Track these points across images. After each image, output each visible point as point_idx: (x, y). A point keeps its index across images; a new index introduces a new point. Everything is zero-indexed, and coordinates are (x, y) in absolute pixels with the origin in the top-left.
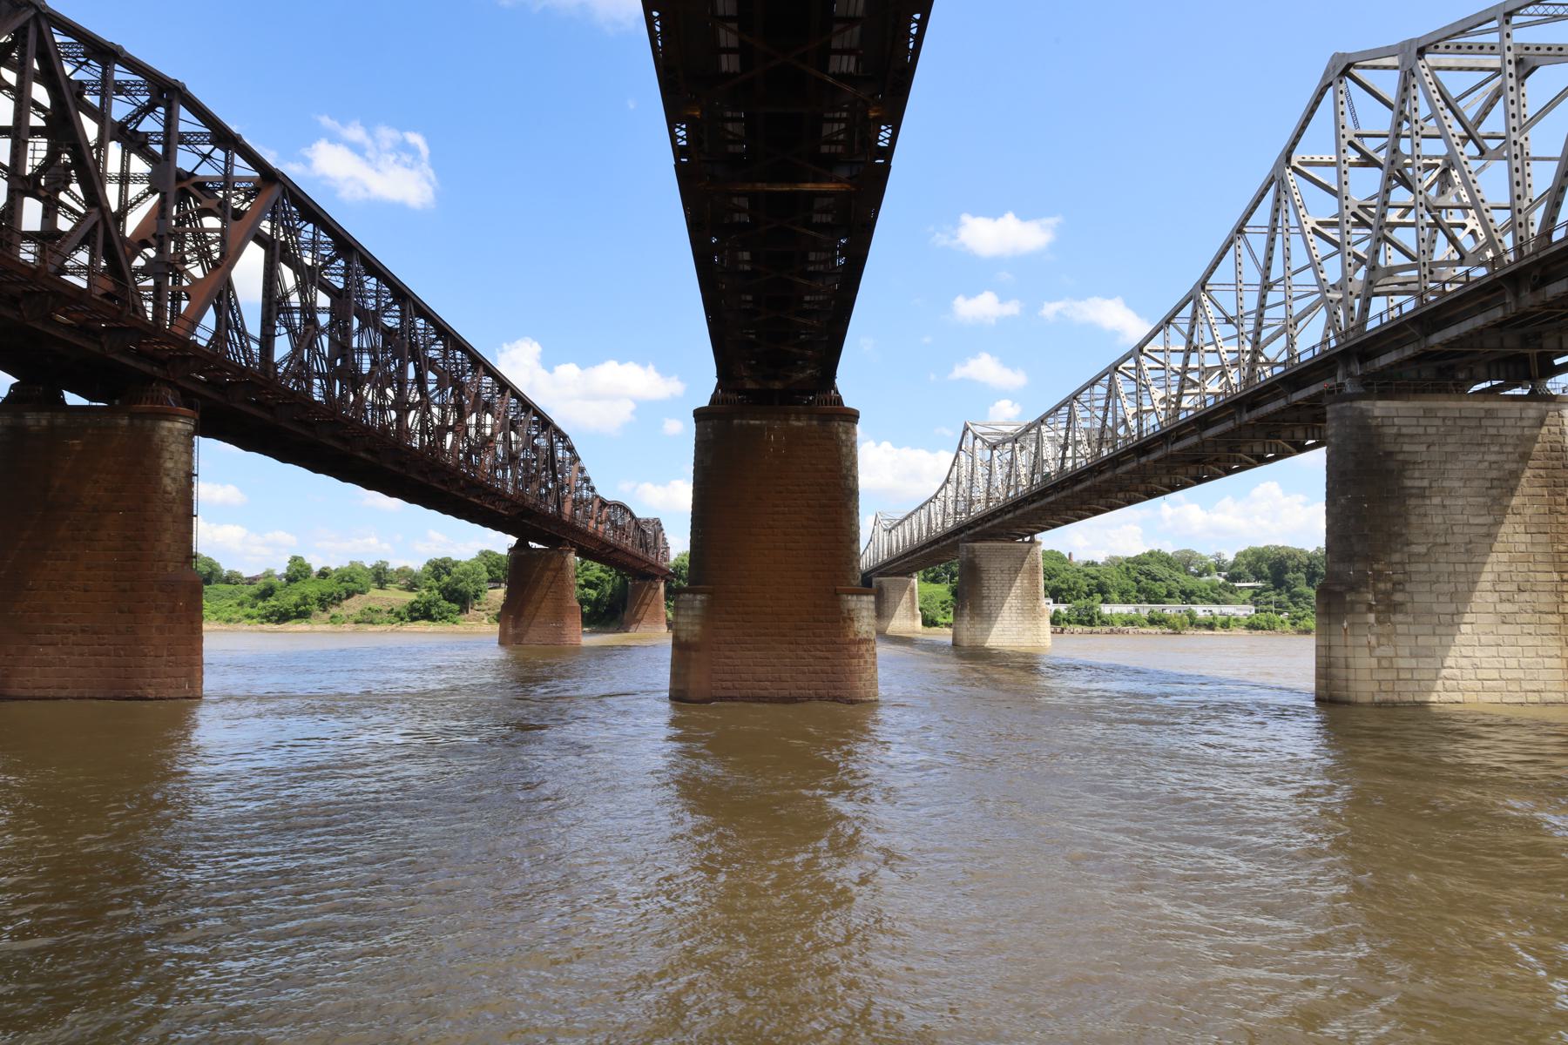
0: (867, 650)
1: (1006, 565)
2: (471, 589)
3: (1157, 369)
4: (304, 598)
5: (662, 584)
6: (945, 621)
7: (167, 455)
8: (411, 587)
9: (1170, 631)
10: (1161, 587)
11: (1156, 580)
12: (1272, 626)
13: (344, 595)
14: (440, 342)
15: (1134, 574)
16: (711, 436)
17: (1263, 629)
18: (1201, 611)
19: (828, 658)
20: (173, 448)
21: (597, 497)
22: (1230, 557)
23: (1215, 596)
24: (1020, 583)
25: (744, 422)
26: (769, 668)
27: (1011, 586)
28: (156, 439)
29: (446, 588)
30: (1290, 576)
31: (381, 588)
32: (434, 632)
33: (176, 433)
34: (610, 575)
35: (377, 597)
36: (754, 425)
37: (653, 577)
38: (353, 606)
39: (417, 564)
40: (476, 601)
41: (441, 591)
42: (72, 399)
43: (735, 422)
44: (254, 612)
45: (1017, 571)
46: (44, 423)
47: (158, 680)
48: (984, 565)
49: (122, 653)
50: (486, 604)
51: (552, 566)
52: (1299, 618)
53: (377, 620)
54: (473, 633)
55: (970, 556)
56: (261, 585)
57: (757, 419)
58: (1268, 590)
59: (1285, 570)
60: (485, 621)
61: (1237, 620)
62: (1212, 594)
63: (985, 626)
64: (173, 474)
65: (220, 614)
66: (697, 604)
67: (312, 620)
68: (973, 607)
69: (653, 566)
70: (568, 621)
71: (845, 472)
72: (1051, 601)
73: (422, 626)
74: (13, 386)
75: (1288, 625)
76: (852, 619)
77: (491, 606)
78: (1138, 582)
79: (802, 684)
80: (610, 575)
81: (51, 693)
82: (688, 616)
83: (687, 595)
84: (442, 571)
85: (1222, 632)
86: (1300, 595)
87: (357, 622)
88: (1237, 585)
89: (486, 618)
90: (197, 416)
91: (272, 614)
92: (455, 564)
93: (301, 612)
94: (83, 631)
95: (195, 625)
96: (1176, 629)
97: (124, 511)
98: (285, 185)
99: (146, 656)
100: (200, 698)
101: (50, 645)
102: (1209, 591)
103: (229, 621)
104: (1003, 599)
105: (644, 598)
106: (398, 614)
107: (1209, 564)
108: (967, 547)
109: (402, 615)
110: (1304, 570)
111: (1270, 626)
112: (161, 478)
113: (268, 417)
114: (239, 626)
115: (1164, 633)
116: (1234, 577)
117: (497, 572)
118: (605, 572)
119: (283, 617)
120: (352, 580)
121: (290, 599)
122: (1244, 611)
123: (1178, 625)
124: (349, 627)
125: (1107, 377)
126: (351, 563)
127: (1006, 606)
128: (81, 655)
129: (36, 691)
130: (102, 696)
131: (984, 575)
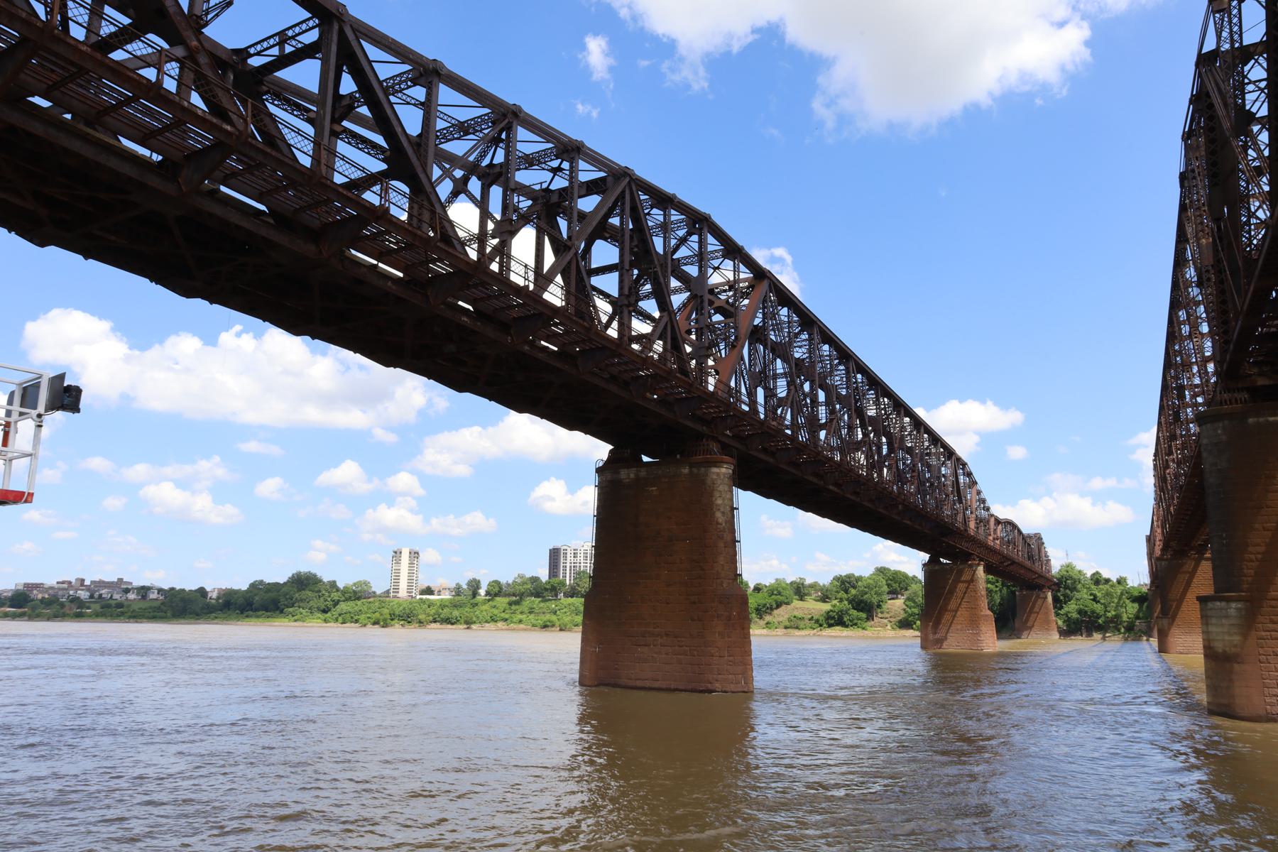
2: (875, 600)
5: (1050, 594)
7: (717, 494)
8: (824, 599)
13: (775, 606)
14: (873, 392)
16: (1224, 438)
20: (721, 488)
21: (992, 515)
25: (1261, 420)
28: (709, 482)
29: (853, 600)
31: (801, 600)
34: (997, 587)
35: (800, 607)
37: (1040, 588)
38: (782, 614)
39: (825, 580)
40: (879, 610)
41: (850, 602)
42: (645, 459)
43: (1251, 420)
46: (632, 476)
49: (695, 653)
50: (888, 613)
51: (963, 579)
53: (801, 626)
54: (881, 638)
60: (889, 627)
64: (722, 509)
66: (1232, 612)
69: (1042, 576)
70: (983, 628)
73: (837, 631)
74: (611, 451)
77: (892, 614)
80: (997, 587)
81: (648, 684)
82: (1222, 625)
83: (1218, 603)
84: (848, 585)
87: (786, 628)
89: (889, 625)
90: (735, 462)
92: (859, 579)
94: (667, 635)
98: (771, 280)
100: (752, 692)
101: (645, 645)
105: (1033, 607)
106: (817, 621)
109: (820, 622)
112: (714, 513)
113: (771, 460)
117: (894, 585)
118: (993, 583)
120: (779, 594)
124: (781, 631)
126: (777, 580)
128: (667, 654)
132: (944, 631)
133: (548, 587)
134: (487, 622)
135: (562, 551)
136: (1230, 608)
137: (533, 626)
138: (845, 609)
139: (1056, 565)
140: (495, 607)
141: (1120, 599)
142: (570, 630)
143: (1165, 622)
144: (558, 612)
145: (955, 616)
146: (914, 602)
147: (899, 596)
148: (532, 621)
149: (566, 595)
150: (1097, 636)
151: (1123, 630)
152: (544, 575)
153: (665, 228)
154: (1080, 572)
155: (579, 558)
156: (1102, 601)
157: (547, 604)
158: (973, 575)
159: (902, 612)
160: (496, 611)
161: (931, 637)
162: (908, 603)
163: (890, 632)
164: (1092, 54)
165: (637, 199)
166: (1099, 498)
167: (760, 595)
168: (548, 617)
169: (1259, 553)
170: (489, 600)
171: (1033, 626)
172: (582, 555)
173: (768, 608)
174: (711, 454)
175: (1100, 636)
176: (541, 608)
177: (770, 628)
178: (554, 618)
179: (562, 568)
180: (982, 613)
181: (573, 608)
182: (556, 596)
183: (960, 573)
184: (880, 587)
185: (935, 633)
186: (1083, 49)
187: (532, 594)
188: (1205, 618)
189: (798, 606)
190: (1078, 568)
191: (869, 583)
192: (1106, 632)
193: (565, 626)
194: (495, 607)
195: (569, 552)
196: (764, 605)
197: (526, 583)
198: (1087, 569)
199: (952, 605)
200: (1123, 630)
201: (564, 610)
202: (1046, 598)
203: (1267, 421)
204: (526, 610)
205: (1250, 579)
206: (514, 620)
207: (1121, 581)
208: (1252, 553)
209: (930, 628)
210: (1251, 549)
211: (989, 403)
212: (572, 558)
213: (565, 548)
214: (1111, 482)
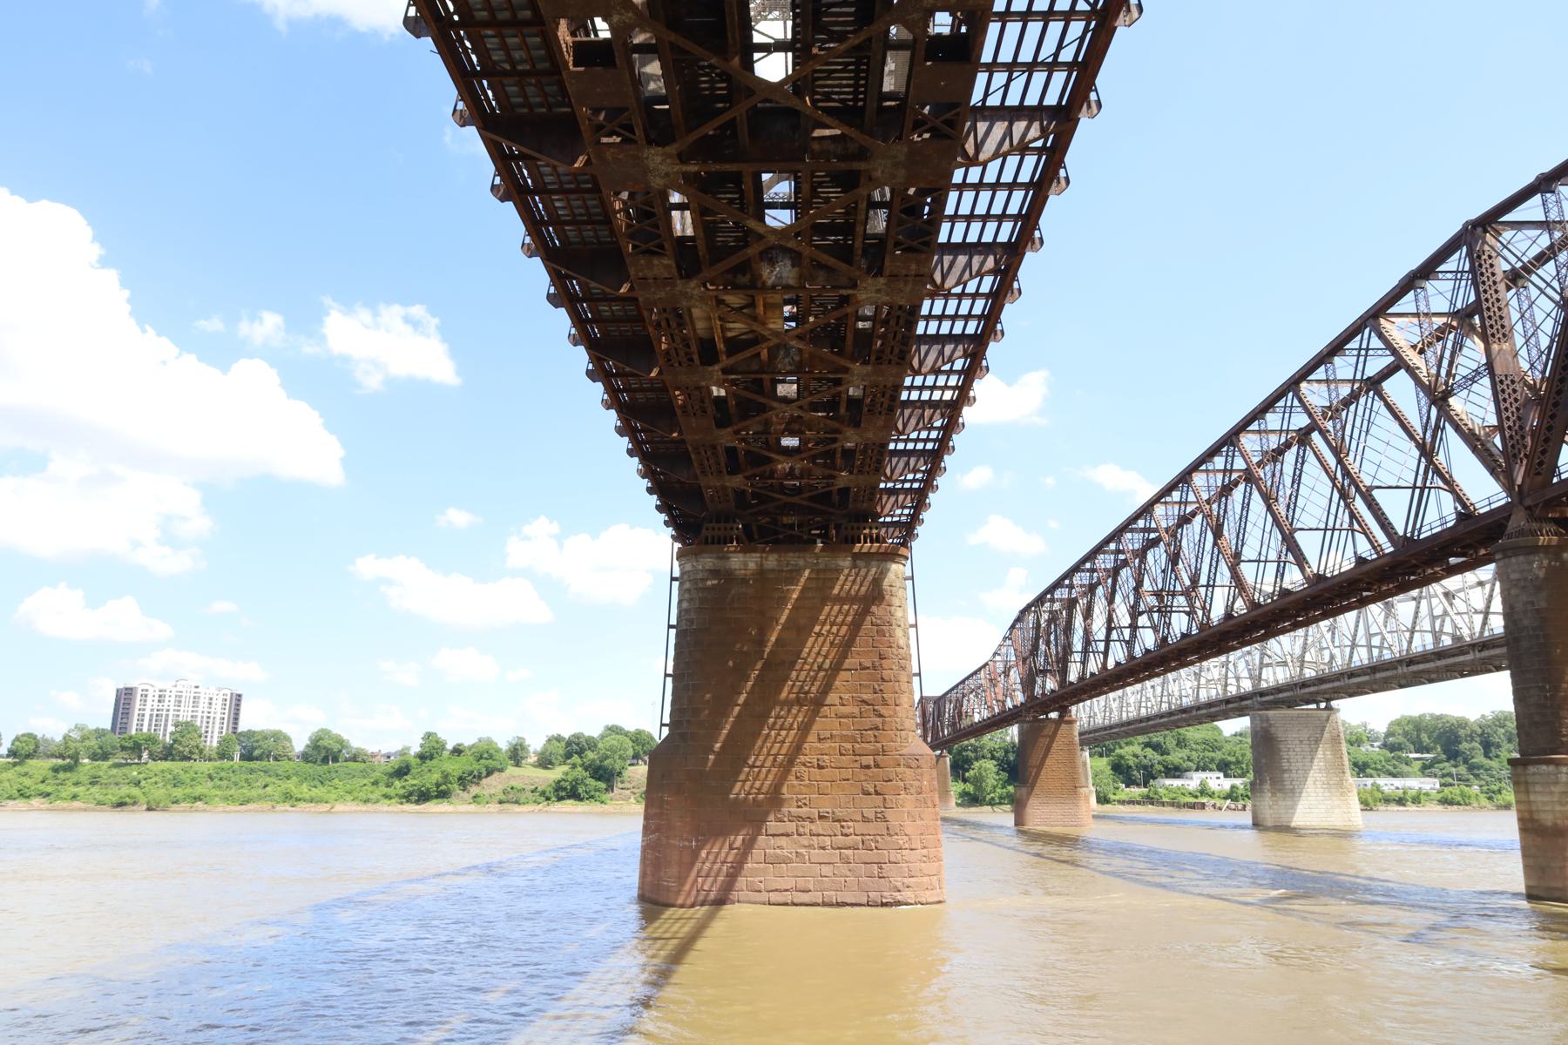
1: (1305, 734)
4: (446, 776)
6: (1117, 798)
12: (1467, 801)
13: (484, 773)
23: (1391, 768)
24: (1323, 754)
27: (1313, 759)
29: (590, 766)
30: (1464, 746)
38: (493, 785)
40: (619, 779)
44: (390, 791)
45: (1317, 742)
46: (752, 565)
48: (1280, 734)
49: (873, 845)
53: (522, 800)
55: (1265, 725)
56: (395, 762)
59: (1457, 740)
60: (632, 800)
61: (1427, 794)
63: (1289, 803)
65: (356, 794)
67: (453, 799)
68: (1274, 782)
72: (1221, 775)
73: (569, 805)
82: (1552, 793)
83: (1544, 767)
86: (1480, 767)
87: (501, 802)
91: (411, 794)
93: (442, 791)
101: (782, 835)
103: (367, 801)
104: (1306, 772)
106: (543, 793)
108: (1260, 715)
109: (547, 794)
110: (1478, 739)
114: (378, 807)
119: (423, 796)
121: (431, 779)
122: (1430, 784)
124: (494, 807)
127: (1310, 781)
131: (1281, 746)
133: (127, 744)
134: (10, 798)
135: (140, 692)
136: (1561, 773)
137: (99, 803)
140: (26, 774)
142: (165, 809)
144: (143, 783)
148: (97, 796)
149: (152, 757)
155: (166, 704)
157: (125, 770)
160: (27, 782)
167: (463, 759)
168: (125, 790)
170: (15, 765)
171: (775, 799)
172: (173, 699)
173: (474, 777)
177: (479, 803)
178: (135, 791)
179: (136, 717)
181: (170, 777)
182: (140, 757)
184: (626, 750)
188: (1520, 784)
189: (515, 774)
194: (26, 774)
195: (150, 694)
196: (471, 773)
201: (153, 780)
204: (85, 779)
206: (64, 795)
212: (156, 703)
213: (145, 687)
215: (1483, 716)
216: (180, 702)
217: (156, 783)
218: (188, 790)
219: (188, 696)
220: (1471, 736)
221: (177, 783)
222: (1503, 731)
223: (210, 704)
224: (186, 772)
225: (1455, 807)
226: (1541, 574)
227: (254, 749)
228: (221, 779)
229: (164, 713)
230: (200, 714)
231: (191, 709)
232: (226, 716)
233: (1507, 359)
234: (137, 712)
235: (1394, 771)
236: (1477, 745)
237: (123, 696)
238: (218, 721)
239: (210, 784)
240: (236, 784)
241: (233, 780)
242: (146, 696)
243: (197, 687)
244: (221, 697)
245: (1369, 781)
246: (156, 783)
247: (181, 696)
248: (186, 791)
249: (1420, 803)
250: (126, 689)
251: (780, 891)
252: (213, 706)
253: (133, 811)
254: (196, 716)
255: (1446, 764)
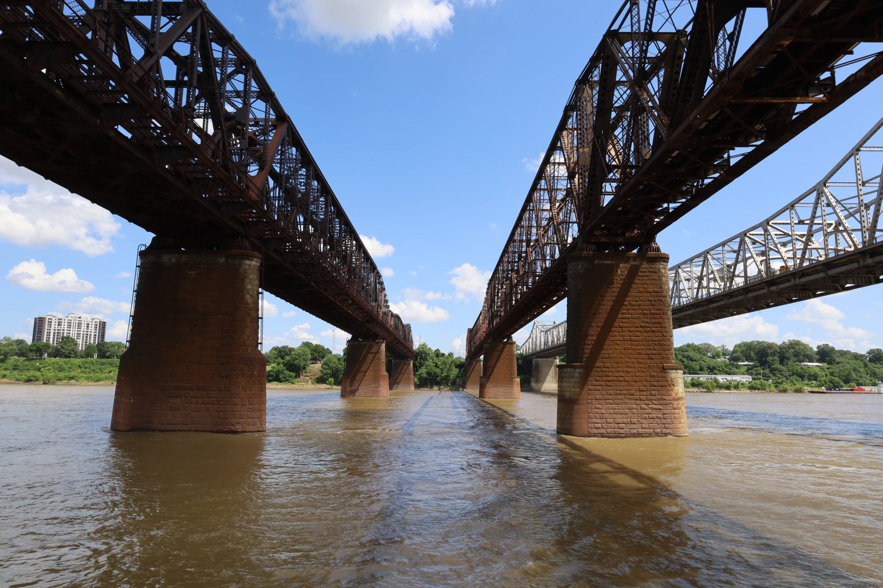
0: (682, 404)
2: (302, 364)
3: (780, 235)
7: (248, 281)
9: (705, 390)
10: (696, 364)
11: (693, 361)
12: (764, 388)
15: (680, 357)
17: (759, 389)
18: (721, 378)
19: (660, 409)
21: (390, 311)
22: (731, 348)
23: (728, 370)
25: (601, 262)
26: (624, 416)
29: (287, 364)
32: (282, 389)
33: (252, 268)
36: (607, 264)
40: (304, 371)
41: (285, 365)
46: (174, 260)
47: (244, 420)
49: (222, 403)
50: (310, 373)
52: (779, 383)
57: (610, 260)
58: (756, 367)
60: (310, 382)
61: (743, 384)
62: (726, 369)
66: (577, 375)
70: (382, 383)
71: (665, 293)
74: (154, 238)
75: (773, 388)
76: (674, 385)
78: (683, 362)
79: (644, 426)
81: (178, 427)
82: (570, 382)
83: (569, 369)
84: (283, 353)
85: (735, 391)
86: (776, 370)
88: (740, 363)
89: (310, 381)
92: (291, 350)
95: (263, 386)
96: (708, 389)
97: (222, 315)
98: (289, 123)
99: (236, 405)
102: (724, 367)
105: (401, 370)
107: (719, 352)
110: (778, 355)
111: (762, 388)
112: (245, 295)
115: (701, 392)
116: (737, 359)
117: (315, 354)
122: (746, 379)
123: (710, 387)
125: (738, 240)
128: (197, 404)
129: (169, 426)
130: (209, 430)
132: (357, 385)
133: (33, 348)
135: (47, 320)
137: (17, 380)
138: (281, 369)
139: (416, 346)
141: (450, 366)
142: (53, 384)
143: (485, 380)
144: (42, 369)
145: (364, 375)
146: (329, 366)
147: (318, 362)
148: (16, 376)
149: (50, 356)
150: (436, 388)
151: (450, 384)
152: (28, 339)
153: (224, 62)
154: (430, 349)
155: (62, 326)
156: (440, 367)
157: (32, 362)
158: (379, 349)
159: (319, 372)
161: (348, 389)
162: (324, 366)
163: (310, 385)
164: (454, 28)
165: (207, 32)
166: (431, 304)
168: (32, 373)
169: (593, 340)
172: (66, 324)
174: (245, 250)
175: (437, 388)
176: (26, 365)
178: (38, 374)
179: (46, 334)
180: (382, 374)
181: (57, 366)
182: (41, 355)
183: (371, 347)
184: (307, 355)
185: (351, 386)
186: (448, 22)
187: (17, 354)
190: (810, 346)
191: (299, 353)
192: (441, 385)
193: (49, 380)
197: (12, 345)
198: (433, 346)
199: (363, 368)
200: (450, 384)
201: (48, 368)
202: (410, 364)
203: (604, 263)
204: (10, 367)
205: (587, 355)
207: (451, 355)
208: (590, 340)
209: (348, 383)
210: (589, 338)
211: (374, 239)
212: (57, 326)
214: (438, 295)
215: (784, 343)
216: (70, 325)
217: (49, 369)
218: (67, 374)
219: (74, 323)
220: (774, 353)
221: (61, 369)
222: (793, 350)
223: (88, 327)
224: (66, 364)
225: (757, 391)
226: (582, 271)
227: (106, 352)
228: (86, 368)
229: (62, 331)
230: (82, 333)
231: (76, 329)
232: (97, 334)
233: (586, 157)
234: (46, 331)
235: (729, 371)
236: (776, 358)
237: (38, 322)
238: (92, 336)
239: (79, 370)
240: (94, 371)
241: (92, 368)
242: (51, 322)
243: (80, 318)
244: (94, 323)
245: (713, 376)
246: (49, 369)
247: (71, 323)
248: (65, 374)
249: (738, 388)
250: (39, 318)
251: (173, 424)
252: (90, 328)
253: (36, 384)
254: (80, 334)
255: (759, 368)
